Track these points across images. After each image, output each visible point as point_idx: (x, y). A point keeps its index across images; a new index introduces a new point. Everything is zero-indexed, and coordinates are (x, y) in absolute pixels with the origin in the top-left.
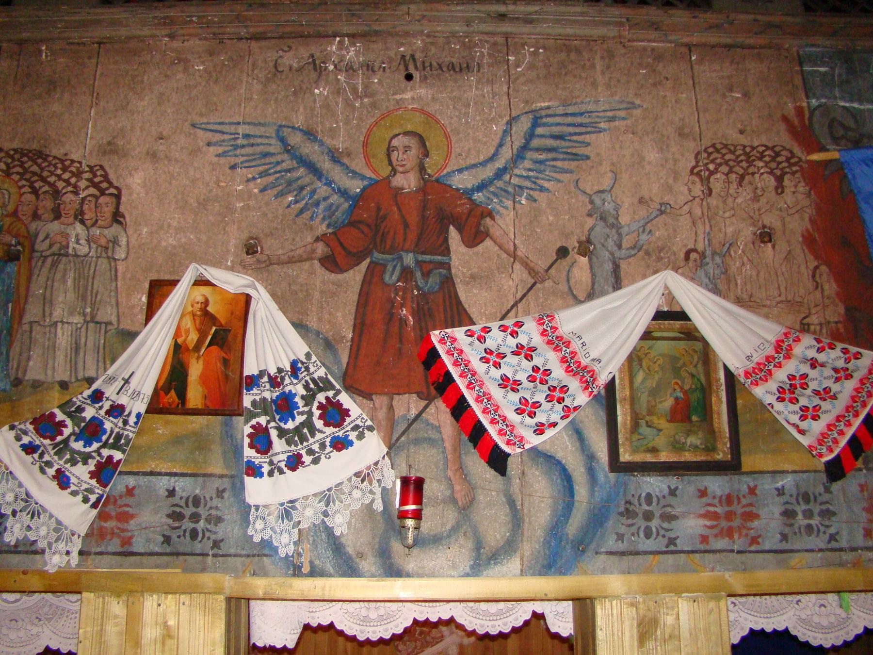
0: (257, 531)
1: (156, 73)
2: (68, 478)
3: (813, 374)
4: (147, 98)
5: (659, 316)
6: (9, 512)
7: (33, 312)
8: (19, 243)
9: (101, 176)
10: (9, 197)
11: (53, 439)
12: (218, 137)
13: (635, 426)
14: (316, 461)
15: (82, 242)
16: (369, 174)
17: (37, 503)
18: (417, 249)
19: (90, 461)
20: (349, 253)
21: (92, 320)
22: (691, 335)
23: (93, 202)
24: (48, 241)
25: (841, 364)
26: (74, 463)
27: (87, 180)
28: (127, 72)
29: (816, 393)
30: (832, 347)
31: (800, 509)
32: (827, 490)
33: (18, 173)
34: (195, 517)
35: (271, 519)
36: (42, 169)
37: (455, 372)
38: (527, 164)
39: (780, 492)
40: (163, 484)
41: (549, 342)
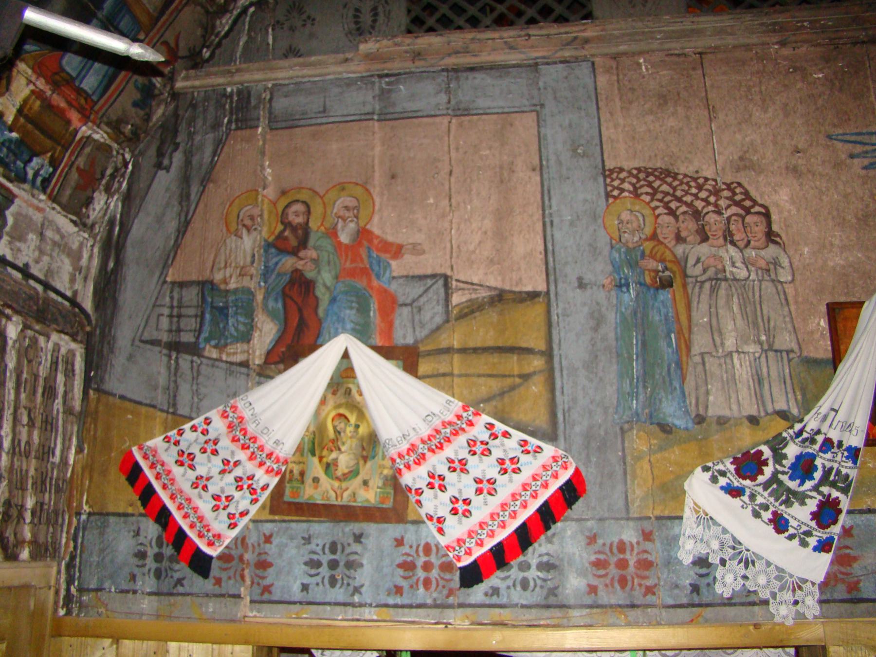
2: (787, 521)
4: (770, 110)
6: (717, 562)
7: (700, 342)
8: (666, 268)
9: (741, 193)
10: (644, 220)
11: (753, 479)
12: (858, 149)
15: (738, 264)
17: (748, 550)
19: (807, 501)
23: (740, 222)
24: (700, 265)
26: (787, 503)
27: (727, 198)
28: (740, 82)
33: (647, 194)
36: (675, 189)
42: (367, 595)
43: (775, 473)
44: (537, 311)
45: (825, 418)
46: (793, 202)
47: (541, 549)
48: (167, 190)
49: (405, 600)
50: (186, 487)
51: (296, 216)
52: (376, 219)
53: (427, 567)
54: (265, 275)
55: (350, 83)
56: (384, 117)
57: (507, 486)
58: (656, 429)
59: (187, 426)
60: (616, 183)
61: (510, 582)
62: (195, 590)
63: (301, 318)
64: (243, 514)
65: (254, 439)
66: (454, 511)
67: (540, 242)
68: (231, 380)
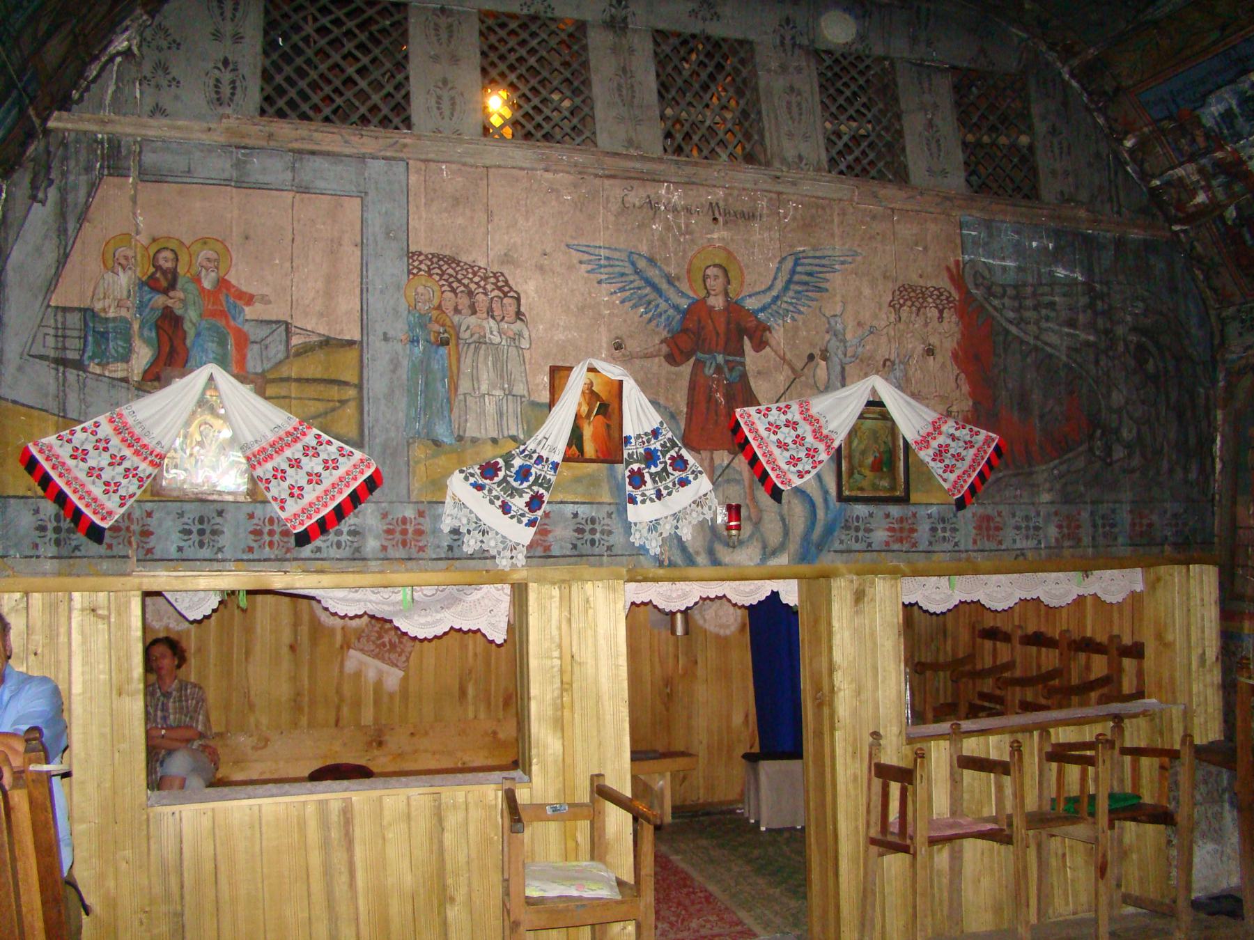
0: (636, 539)
1: (536, 199)
3: (953, 444)
5: (869, 404)
7: (464, 385)
8: (445, 331)
11: (491, 479)
12: (586, 257)
13: (851, 474)
14: (670, 494)
16: (691, 294)
18: (726, 352)
20: (682, 352)
21: (510, 393)
22: (886, 416)
25: (968, 438)
26: (512, 495)
29: (953, 456)
30: (964, 427)
31: (940, 526)
32: (955, 516)
34: (593, 531)
35: (645, 531)
36: (457, 273)
37: (750, 437)
38: (791, 293)
39: (930, 516)
40: (569, 509)
41: (805, 419)
42: (228, 553)
43: (505, 476)
44: (352, 354)
45: (540, 443)
46: (537, 292)
47: (350, 521)
48: (45, 223)
49: (256, 557)
50: (82, 476)
51: (166, 260)
52: (233, 271)
53: (271, 533)
54: (141, 307)
55: (210, 149)
56: (240, 184)
57: (329, 478)
58: (430, 442)
59: (78, 428)
60: (416, 263)
61: (328, 543)
62: (91, 554)
63: (172, 346)
64: (131, 496)
65: (138, 440)
66: (292, 495)
67: (358, 301)
68: (113, 392)
